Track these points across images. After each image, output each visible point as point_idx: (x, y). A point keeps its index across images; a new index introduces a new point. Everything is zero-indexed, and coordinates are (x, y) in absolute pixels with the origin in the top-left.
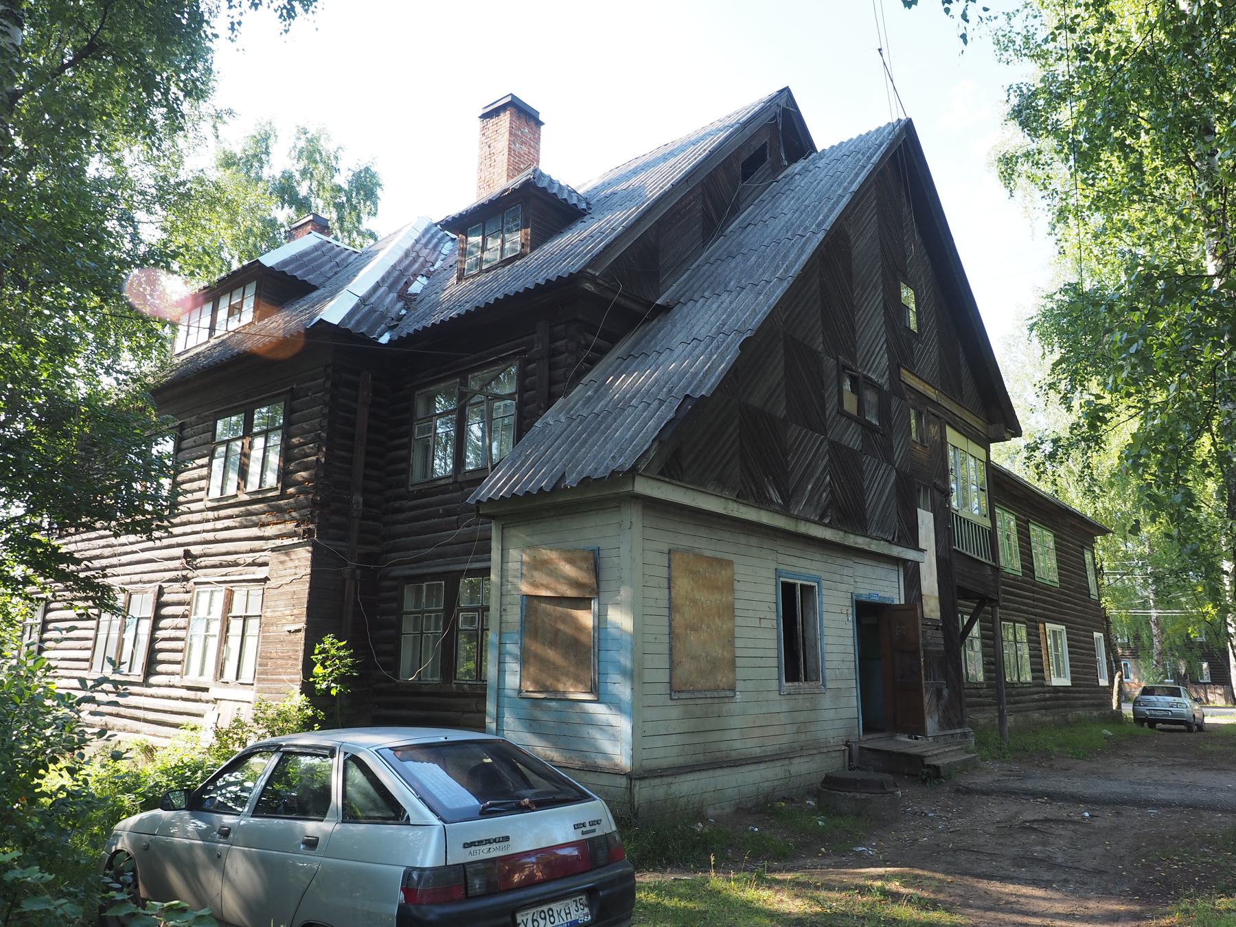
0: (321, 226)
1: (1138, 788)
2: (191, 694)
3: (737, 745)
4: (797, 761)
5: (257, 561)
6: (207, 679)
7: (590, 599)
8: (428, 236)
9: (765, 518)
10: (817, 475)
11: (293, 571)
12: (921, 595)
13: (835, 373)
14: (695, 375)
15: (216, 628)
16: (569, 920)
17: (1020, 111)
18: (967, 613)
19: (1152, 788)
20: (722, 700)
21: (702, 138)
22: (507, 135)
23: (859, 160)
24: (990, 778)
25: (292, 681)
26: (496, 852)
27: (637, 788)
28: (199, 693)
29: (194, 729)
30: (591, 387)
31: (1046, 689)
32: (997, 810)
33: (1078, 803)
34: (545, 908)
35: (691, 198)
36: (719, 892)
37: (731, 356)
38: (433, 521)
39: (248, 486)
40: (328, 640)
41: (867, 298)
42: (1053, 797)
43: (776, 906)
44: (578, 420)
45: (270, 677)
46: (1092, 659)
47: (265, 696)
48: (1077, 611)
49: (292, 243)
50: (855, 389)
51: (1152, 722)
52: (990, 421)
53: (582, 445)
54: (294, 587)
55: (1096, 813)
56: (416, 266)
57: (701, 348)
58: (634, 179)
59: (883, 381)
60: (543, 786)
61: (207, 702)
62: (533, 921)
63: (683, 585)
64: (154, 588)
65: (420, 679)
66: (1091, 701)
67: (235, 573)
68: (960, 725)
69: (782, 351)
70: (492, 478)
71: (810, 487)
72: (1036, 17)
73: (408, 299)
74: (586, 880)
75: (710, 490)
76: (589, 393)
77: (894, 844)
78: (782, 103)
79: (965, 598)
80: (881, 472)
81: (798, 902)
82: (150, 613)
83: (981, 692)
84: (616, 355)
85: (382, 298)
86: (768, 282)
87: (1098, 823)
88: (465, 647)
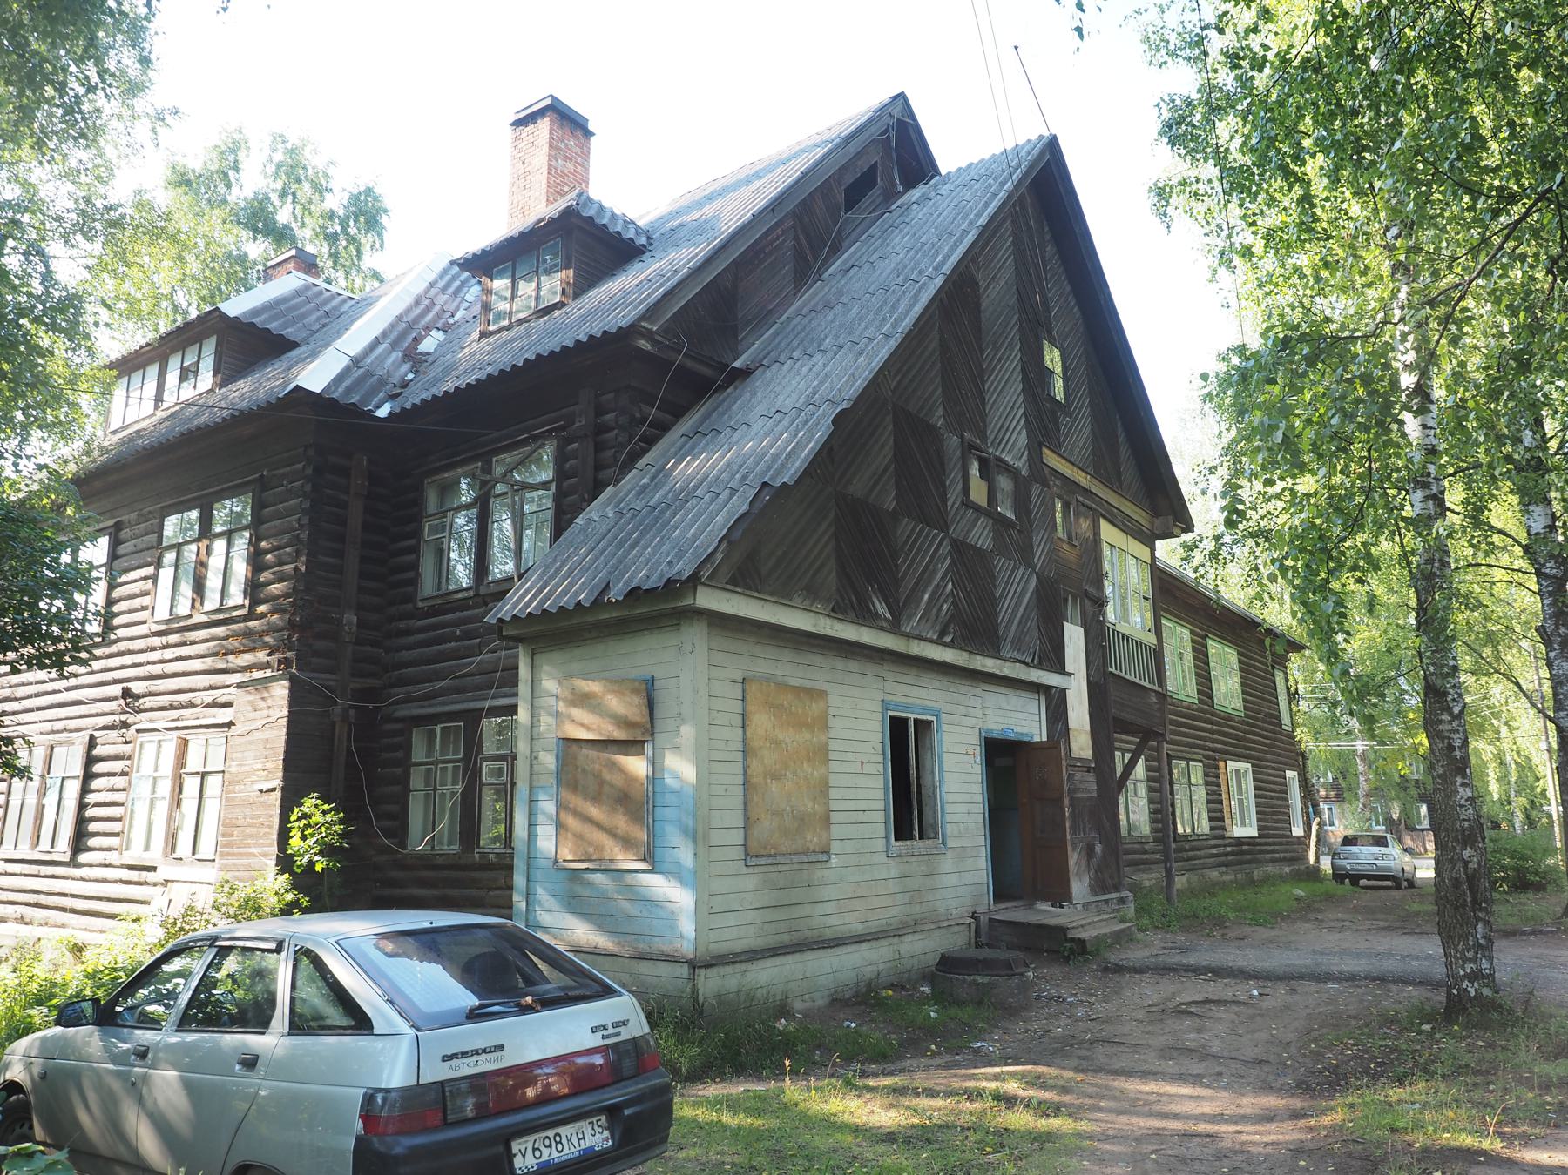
0: (308, 264)
1: (1320, 958)
2: (134, 876)
3: (832, 921)
4: (909, 938)
5: (219, 700)
6: (155, 856)
7: (643, 742)
8: (447, 278)
9: (866, 636)
10: (935, 582)
11: (265, 712)
12: (1068, 730)
13: (958, 453)
14: (776, 457)
15: (165, 788)
16: (583, 1147)
17: (1170, 127)
18: (1128, 751)
19: (1336, 959)
20: (812, 866)
21: (795, 156)
22: (546, 148)
23: (990, 186)
24: (1146, 953)
25: (264, 855)
26: (486, 1064)
27: (702, 978)
28: (144, 874)
29: (138, 920)
30: (648, 473)
31: (1227, 841)
32: (1150, 991)
33: (1247, 979)
34: (551, 1133)
35: (779, 231)
36: (796, 1104)
37: (821, 434)
38: (448, 645)
39: (206, 603)
40: (310, 803)
41: (1000, 360)
42: (1218, 972)
43: (865, 1119)
44: (629, 515)
45: (236, 850)
46: (1284, 803)
47: (229, 876)
48: (1266, 745)
49: (269, 284)
50: (985, 474)
51: (1355, 879)
52: (1155, 512)
53: (633, 547)
54: (267, 734)
55: (1267, 991)
56: (430, 317)
57: (785, 423)
58: (708, 207)
59: (1021, 464)
60: (555, 980)
61: (155, 885)
62: (534, 1150)
63: (762, 722)
64: (83, 738)
65: (433, 849)
66: (1282, 855)
67: (189, 717)
68: (1117, 889)
69: (891, 428)
70: (518, 589)
71: (926, 597)
72: (1194, 10)
73: (416, 360)
74: (617, 1093)
75: (797, 601)
76: (645, 480)
77: (1021, 1037)
78: (896, 112)
79: (1127, 733)
80: (1018, 577)
81: (893, 1113)
82: (78, 769)
83: (1147, 847)
84: (680, 433)
85: (381, 359)
86: (871, 340)
87: (1267, 1003)
88: (489, 805)
